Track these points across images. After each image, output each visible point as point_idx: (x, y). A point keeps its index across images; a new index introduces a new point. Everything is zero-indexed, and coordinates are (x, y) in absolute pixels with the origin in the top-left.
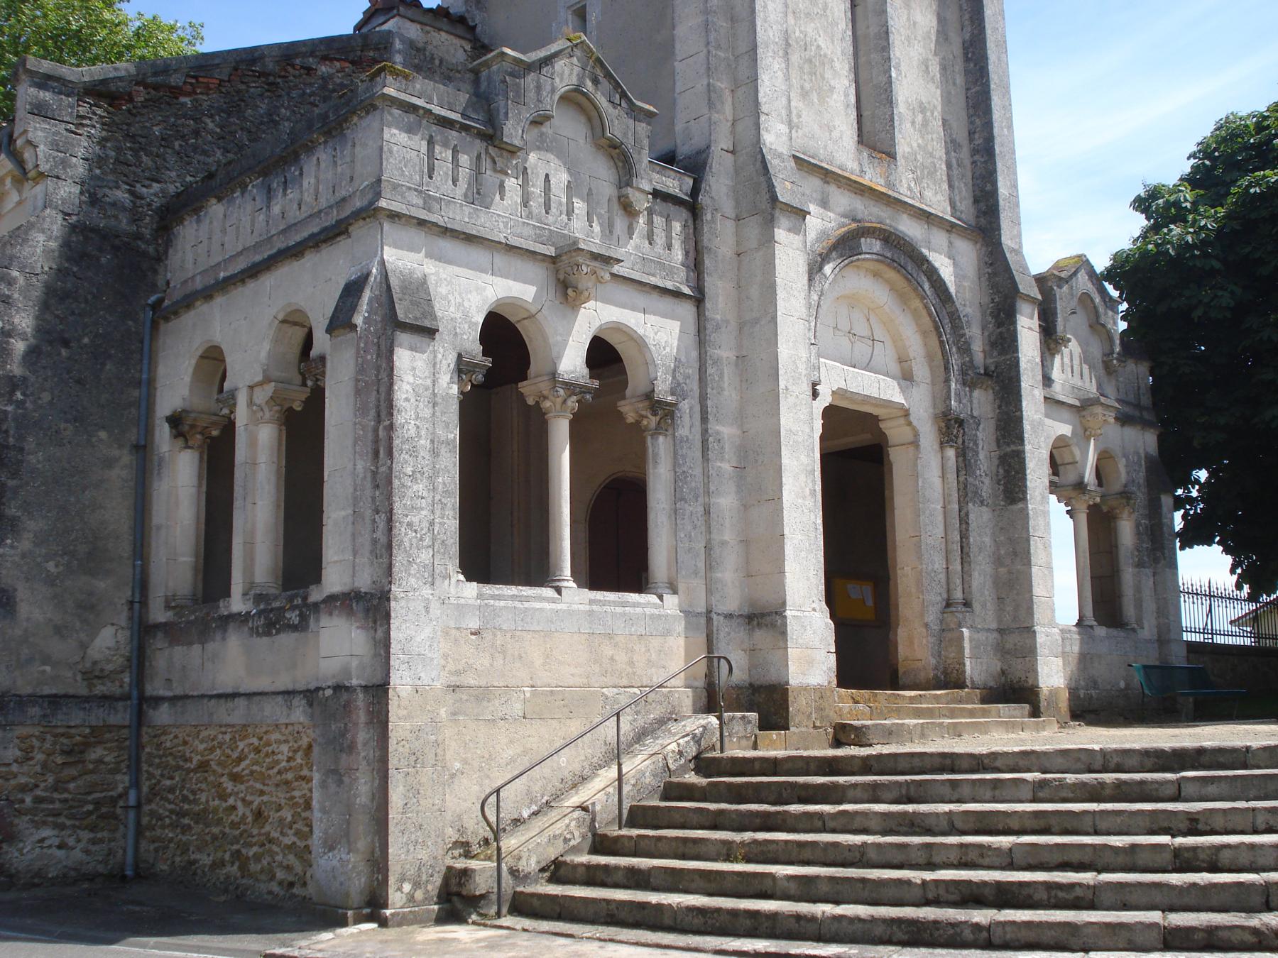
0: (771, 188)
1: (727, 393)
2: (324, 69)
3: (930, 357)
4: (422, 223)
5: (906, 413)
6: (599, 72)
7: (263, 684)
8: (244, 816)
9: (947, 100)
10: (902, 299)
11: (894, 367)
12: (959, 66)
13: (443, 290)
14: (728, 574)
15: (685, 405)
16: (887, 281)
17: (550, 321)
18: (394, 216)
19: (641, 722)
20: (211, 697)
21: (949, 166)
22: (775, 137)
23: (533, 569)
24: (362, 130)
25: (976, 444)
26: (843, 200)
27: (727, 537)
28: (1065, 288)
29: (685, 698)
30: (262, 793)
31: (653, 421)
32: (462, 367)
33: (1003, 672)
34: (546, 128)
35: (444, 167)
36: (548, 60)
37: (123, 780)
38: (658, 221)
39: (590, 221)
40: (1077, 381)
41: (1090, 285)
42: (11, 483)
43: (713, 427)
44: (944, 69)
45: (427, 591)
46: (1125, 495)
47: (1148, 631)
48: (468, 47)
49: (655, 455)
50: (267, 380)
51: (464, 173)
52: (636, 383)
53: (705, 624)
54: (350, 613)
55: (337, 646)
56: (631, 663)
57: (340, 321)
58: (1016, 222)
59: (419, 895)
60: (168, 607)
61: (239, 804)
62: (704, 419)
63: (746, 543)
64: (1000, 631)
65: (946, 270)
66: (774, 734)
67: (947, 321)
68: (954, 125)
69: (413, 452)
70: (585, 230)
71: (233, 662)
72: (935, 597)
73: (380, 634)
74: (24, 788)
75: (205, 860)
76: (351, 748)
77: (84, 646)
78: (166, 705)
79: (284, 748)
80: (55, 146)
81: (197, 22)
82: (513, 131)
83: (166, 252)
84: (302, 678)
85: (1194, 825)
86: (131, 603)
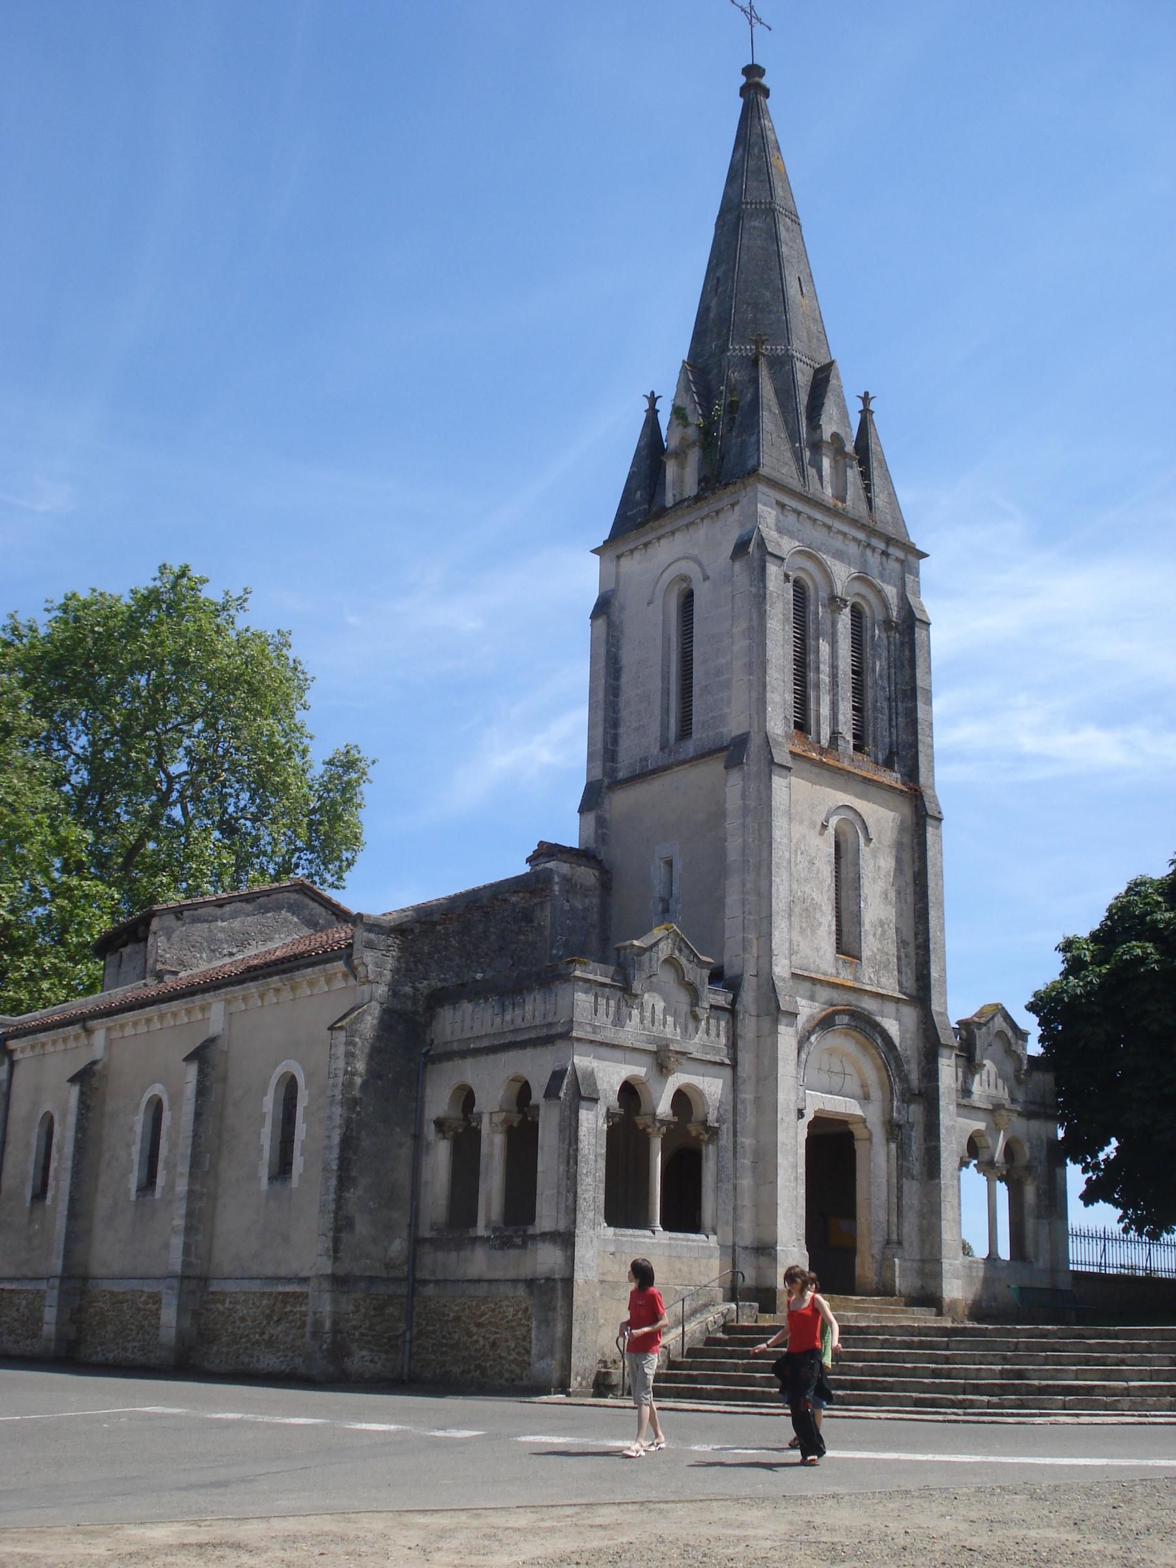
0: (777, 1001)
1: (749, 1119)
2: (514, 899)
3: (882, 1085)
4: (592, 1042)
5: (864, 1121)
6: (682, 945)
7: (498, 1275)
8: (484, 1346)
9: (900, 915)
10: (864, 1049)
11: (858, 1091)
12: (910, 889)
13: (601, 1075)
14: (746, 1224)
15: (724, 1128)
16: (854, 1038)
17: (653, 1086)
18: (579, 1040)
19: (694, 1305)
20: (464, 1281)
21: (899, 958)
22: (781, 969)
23: (639, 1220)
24: (561, 989)
25: (910, 1140)
26: (824, 994)
27: (745, 1203)
28: (984, 1029)
29: (719, 1293)
30: (497, 1333)
31: (707, 1136)
32: (609, 1115)
33: (922, 1287)
34: (654, 979)
35: (602, 1009)
36: (656, 944)
37: (402, 1326)
38: (712, 1021)
39: (675, 1027)
40: (993, 1091)
41: (1004, 1024)
42: (354, 1158)
43: (740, 1139)
44: (898, 893)
45: (591, 1232)
46: (1029, 1168)
47: (1043, 1262)
48: (597, 874)
49: (707, 1156)
50: (501, 1111)
51: (612, 1010)
52: (697, 1114)
53: (731, 1252)
54: (554, 1242)
55: (547, 1258)
56: (691, 1273)
57: (552, 1092)
58: (944, 993)
59: (584, 1383)
60: (432, 1229)
61: (481, 1339)
62: (735, 1135)
63: (756, 1206)
64: (923, 1261)
65: (892, 1027)
66: (767, 1316)
67: (892, 1062)
68: (904, 930)
69: (587, 1162)
70: (670, 1031)
71: (479, 1263)
72: (879, 1238)
73: (569, 1253)
74: (355, 1328)
75: (456, 1370)
76: (554, 1309)
77: (386, 1249)
78: (432, 1285)
79: (511, 1309)
80: (377, 965)
81: (284, 630)
82: (637, 987)
83: (431, 1022)
84: (525, 1272)
85: (947, 1360)
86: (410, 1225)
